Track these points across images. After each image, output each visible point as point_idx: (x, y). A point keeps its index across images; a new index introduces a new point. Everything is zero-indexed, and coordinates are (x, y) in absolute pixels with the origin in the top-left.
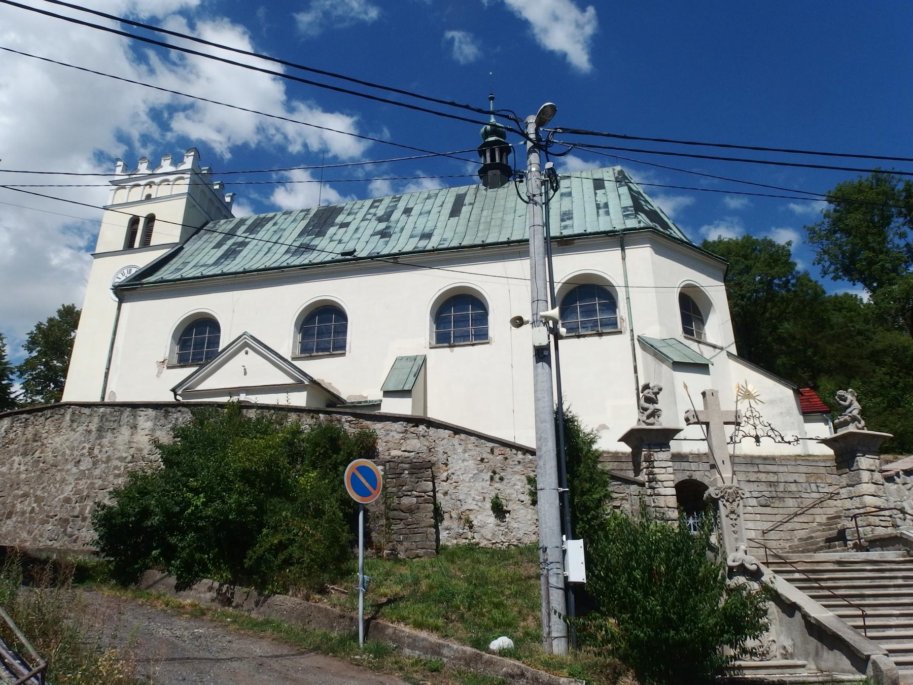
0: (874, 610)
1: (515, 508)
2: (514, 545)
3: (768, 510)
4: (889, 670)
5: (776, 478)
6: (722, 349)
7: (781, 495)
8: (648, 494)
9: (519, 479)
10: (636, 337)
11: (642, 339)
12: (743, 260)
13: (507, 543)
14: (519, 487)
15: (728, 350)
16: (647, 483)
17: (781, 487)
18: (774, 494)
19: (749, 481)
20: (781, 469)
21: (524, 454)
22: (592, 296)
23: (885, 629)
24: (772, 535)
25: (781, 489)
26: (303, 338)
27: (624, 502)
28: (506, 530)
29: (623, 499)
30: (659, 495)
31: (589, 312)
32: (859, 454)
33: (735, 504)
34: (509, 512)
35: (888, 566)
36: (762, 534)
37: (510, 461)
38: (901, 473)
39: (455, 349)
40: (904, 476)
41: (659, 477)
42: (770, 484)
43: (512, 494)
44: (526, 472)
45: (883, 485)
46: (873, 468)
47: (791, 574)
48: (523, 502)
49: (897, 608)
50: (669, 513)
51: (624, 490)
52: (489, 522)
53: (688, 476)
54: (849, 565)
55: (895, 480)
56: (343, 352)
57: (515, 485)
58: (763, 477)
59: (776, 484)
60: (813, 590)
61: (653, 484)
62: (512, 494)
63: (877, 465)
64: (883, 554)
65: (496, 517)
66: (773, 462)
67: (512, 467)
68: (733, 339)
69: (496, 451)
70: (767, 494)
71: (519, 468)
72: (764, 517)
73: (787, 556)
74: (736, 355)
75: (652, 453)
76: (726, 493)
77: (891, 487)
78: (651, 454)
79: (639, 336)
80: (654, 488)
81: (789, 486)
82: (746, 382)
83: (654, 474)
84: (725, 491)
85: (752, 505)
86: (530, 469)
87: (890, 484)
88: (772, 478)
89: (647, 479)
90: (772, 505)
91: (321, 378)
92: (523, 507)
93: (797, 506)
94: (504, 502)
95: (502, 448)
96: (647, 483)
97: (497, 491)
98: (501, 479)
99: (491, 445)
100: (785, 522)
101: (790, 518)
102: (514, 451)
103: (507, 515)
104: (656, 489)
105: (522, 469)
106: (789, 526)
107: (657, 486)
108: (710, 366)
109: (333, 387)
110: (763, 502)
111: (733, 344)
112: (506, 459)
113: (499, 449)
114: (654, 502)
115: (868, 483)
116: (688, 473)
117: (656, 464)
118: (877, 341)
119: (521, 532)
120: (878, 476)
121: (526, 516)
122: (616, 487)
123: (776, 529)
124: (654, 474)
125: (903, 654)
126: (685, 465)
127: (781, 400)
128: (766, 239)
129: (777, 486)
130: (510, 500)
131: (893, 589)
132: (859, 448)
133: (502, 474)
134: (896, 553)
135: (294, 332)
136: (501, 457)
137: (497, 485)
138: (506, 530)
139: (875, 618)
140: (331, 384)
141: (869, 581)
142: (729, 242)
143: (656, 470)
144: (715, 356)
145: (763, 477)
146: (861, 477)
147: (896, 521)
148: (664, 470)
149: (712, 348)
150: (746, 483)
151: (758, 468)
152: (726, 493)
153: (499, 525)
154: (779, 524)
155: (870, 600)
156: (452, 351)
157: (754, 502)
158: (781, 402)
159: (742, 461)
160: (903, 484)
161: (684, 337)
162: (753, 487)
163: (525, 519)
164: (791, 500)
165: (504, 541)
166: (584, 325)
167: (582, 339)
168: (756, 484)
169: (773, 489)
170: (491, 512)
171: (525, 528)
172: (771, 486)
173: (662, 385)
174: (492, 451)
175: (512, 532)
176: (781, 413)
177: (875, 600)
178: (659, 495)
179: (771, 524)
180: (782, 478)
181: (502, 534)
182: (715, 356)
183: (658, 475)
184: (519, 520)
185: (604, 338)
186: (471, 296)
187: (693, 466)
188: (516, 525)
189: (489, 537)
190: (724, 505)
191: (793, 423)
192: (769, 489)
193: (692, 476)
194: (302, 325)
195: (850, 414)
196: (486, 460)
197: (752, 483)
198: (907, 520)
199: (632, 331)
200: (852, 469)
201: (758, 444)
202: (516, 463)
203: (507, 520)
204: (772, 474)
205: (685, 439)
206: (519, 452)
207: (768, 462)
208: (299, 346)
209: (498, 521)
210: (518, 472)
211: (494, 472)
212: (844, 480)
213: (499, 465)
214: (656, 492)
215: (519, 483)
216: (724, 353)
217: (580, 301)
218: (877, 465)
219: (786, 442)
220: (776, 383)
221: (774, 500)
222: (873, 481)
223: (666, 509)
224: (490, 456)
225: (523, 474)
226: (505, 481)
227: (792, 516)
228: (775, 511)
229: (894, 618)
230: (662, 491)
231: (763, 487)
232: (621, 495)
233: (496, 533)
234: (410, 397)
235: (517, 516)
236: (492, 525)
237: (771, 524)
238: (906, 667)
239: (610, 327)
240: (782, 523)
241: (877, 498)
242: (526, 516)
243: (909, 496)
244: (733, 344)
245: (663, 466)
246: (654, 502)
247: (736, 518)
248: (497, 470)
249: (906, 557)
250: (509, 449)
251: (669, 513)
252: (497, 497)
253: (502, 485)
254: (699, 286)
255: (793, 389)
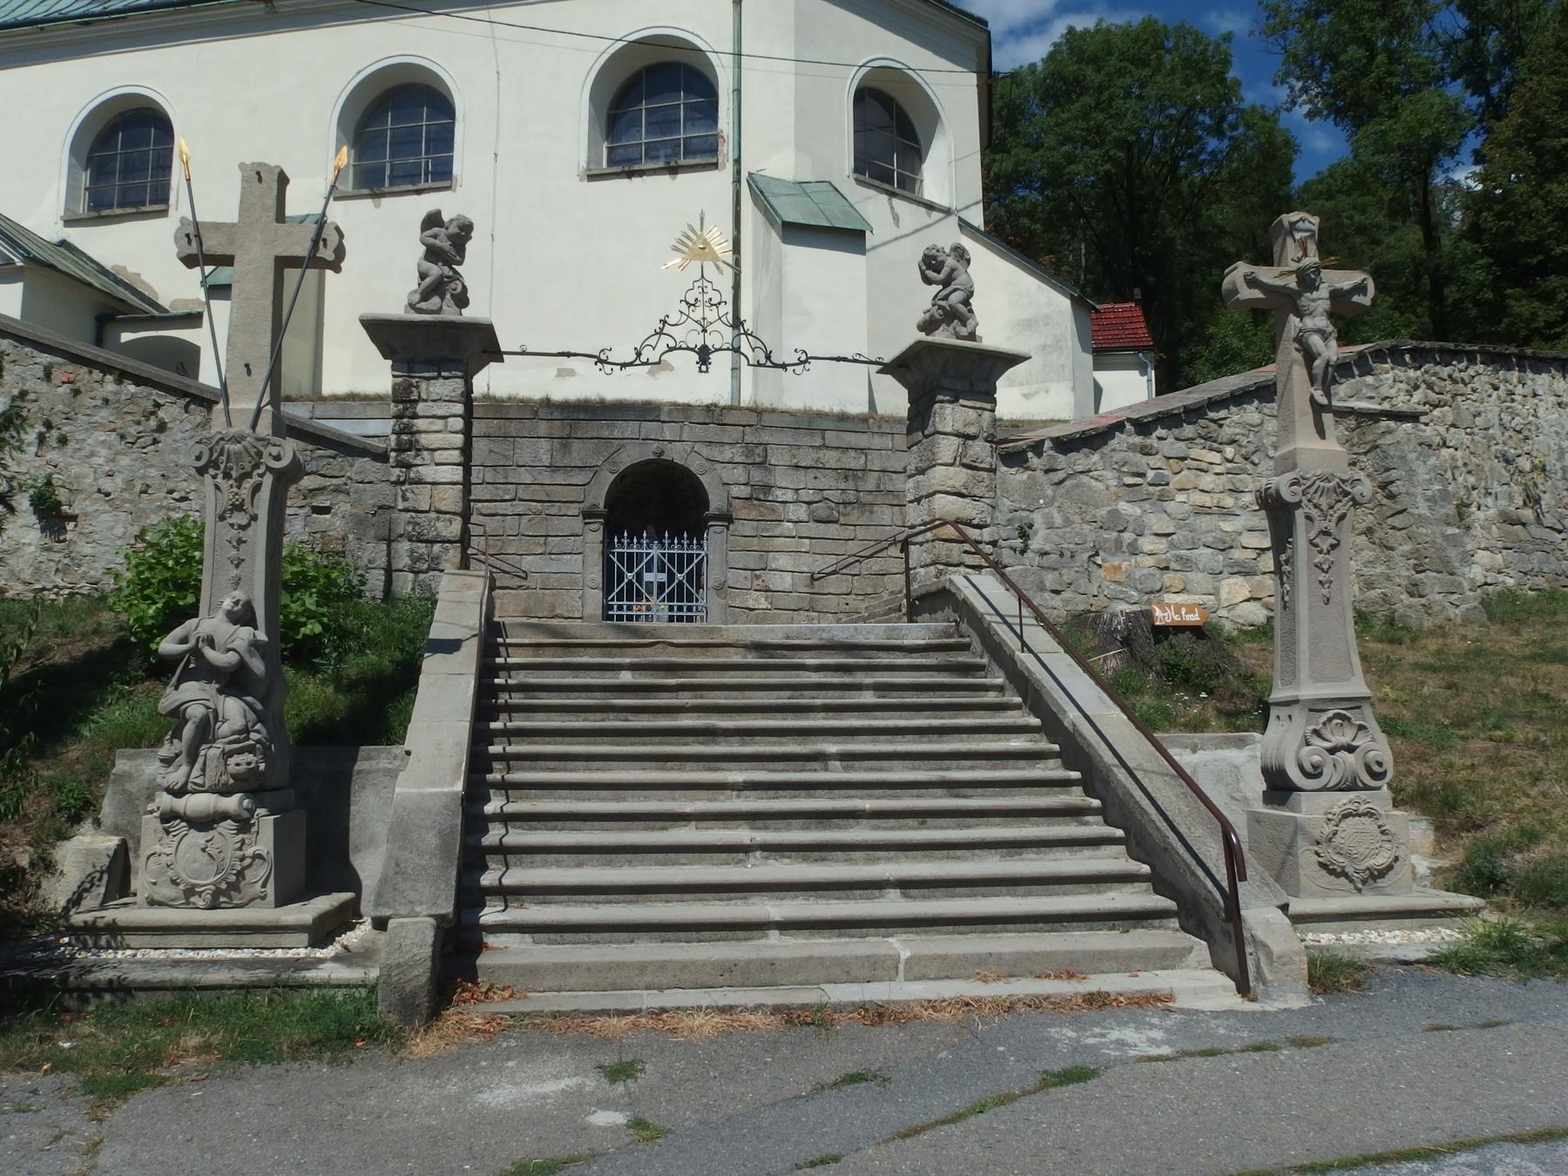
0: (710, 769)
1: (90, 509)
2: (82, 594)
3: (832, 530)
4: (399, 965)
5: (862, 460)
6: (947, 212)
7: (869, 498)
8: (393, 479)
9: (103, 442)
10: (744, 175)
11: (754, 181)
12: (1132, 68)
13: (67, 591)
14: (101, 461)
15: (964, 215)
16: (393, 454)
17: (871, 482)
18: (851, 497)
19: (797, 467)
20: (878, 442)
21: (119, 382)
22: (673, 89)
23: (668, 824)
24: (832, 584)
25: (871, 485)
26: (95, 178)
27: (341, 497)
28: (66, 561)
29: (337, 490)
30: (420, 482)
31: (663, 122)
32: (940, 397)
33: (248, 484)
34: (74, 518)
35: (885, 659)
36: (809, 581)
37: (85, 399)
38: (1048, 444)
39: (385, 201)
40: (1052, 452)
41: (424, 440)
42: (847, 473)
43: (86, 476)
44: (119, 424)
45: (993, 470)
46: (972, 430)
47: (610, 674)
48: (108, 494)
49: (771, 765)
50: (439, 525)
51: (342, 469)
52: (26, 541)
53: (655, 453)
54: (785, 652)
55: (1027, 461)
56: (162, 207)
57: (92, 454)
58: (831, 458)
59: (860, 474)
60: (611, 715)
61: (409, 456)
62: (86, 476)
63: (985, 425)
64: (895, 629)
65: (43, 530)
66: (860, 427)
67: (88, 412)
68: (978, 193)
69: (58, 376)
70: (835, 496)
71: (104, 415)
72: (820, 546)
73: (564, 627)
74: (982, 229)
75: (414, 381)
76: (221, 453)
77: (1014, 477)
78: (411, 385)
79: (750, 174)
80: (409, 466)
81: (891, 480)
82: (702, 219)
83: (413, 433)
84: (218, 448)
85: (794, 518)
86: (130, 417)
87: (1013, 470)
88: (853, 461)
89: (393, 444)
90: (842, 520)
91: (121, 264)
92: (107, 507)
93: (900, 523)
94: (62, 494)
95: (71, 368)
96: (393, 454)
97: (49, 469)
98: (63, 441)
99: (46, 359)
100: (867, 557)
101: (879, 547)
102: (97, 375)
103: (70, 526)
104: (414, 469)
105: (111, 418)
106: (875, 565)
107: (418, 461)
108: (868, 233)
109: (143, 282)
110: (821, 510)
111: (977, 203)
112: (77, 392)
113: (64, 368)
114: (405, 499)
115: (952, 465)
116: (655, 445)
117: (421, 408)
118: (1389, 248)
119: (100, 566)
120: (980, 450)
121: (111, 529)
122: (325, 461)
123: (844, 571)
124: (413, 433)
125: (630, 897)
126: (649, 428)
127: (1047, 320)
128: (1183, 26)
129: (862, 478)
130: (79, 491)
131: (822, 714)
132: (946, 383)
133: (66, 429)
134: (928, 628)
135: (70, 167)
136: (65, 389)
137: (53, 455)
138: (66, 561)
139: (677, 793)
140: (139, 275)
141: (789, 693)
142: (1126, 32)
143: (420, 424)
144: (928, 226)
145: (831, 458)
146: (935, 450)
147: (1000, 555)
148: (441, 422)
149: (923, 210)
150: (791, 472)
151: (824, 438)
152: (221, 453)
153: (49, 549)
154: (851, 560)
155: (730, 744)
156: (377, 206)
157: (801, 512)
158: (1046, 325)
159: (788, 421)
160: (1047, 472)
161: (857, 180)
162: (801, 479)
163: (109, 535)
164: (887, 510)
165: (62, 584)
166: (652, 151)
167: (636, 180)
168: (811, 473)
169: (850, 484)
170: (33, 519)
171: (108, 556)
172: (846, 478)
173: (472, 216)
174: (48, 375)
175: (79, 566)
176: (1045, 346)
177: (744, 744)
178: (420, 482)
179: (833, 559)
180: (876, 462)
181: (57, 570)
182: (928, 226)
183: (423, 435)
184: (96, 537)
185: (682, 178)
186: (428, 87)
187: (669, 431)
188: (87, 550)
189: (27, 575)
190: (217, 487)
191: (1063, 367)
192: (843, 486)
193: (662, 453)
194: (94, 149)
195: (943, 303)
196: (32, 396)
197: (802, 472)
198: (1029, 554)
199: (738, 162)
200: (926, 432)
201: (704, 368)
202: (99, 403)
203: (68, 536)
204: (853, 453)
205: (524, 353)
206: (109, 378)
207: (848, 426)
208: (83, 197)
209: (47, 540)
210: (102, 425)
211: (49, 425)
212: (912, 460)
213: (61, 407)
214: (412, 475)
215: (103, 452)
216: (953, 220)
217: (649, 98)
218: (985, 425)
219: (775, 366)
220: (1043, 285)
221: (849, 508)
222: (964, 461)
223: (433, 515)
224: (43, 387)
225: (114, 430)
226: (71, 445)
227: (885, 544)
228: (848, 532)
229: (729, 792)
230: (428, 472)
231: (827, 481)
232: (334, 481)
233: (43, 566)
234: (228, 298)
235: (91, 529)
236: (32, 548)
237: (833, 559)
238: (594, 936)
239: (703, 154)
240: (860, 559)
241: (968, 500)
242: (111, 529)
243: (1053, 500)
244: (977, 203)
245: (440, 413)
246: (405, 499)
247: (244, 522)
248: (55, 420)
249: (950, 636)
250: (85, 369)
251: (439, 525)
252: (49, 483)
253: (64, 454)
254: (899, 66)
255: (1072, 298)
